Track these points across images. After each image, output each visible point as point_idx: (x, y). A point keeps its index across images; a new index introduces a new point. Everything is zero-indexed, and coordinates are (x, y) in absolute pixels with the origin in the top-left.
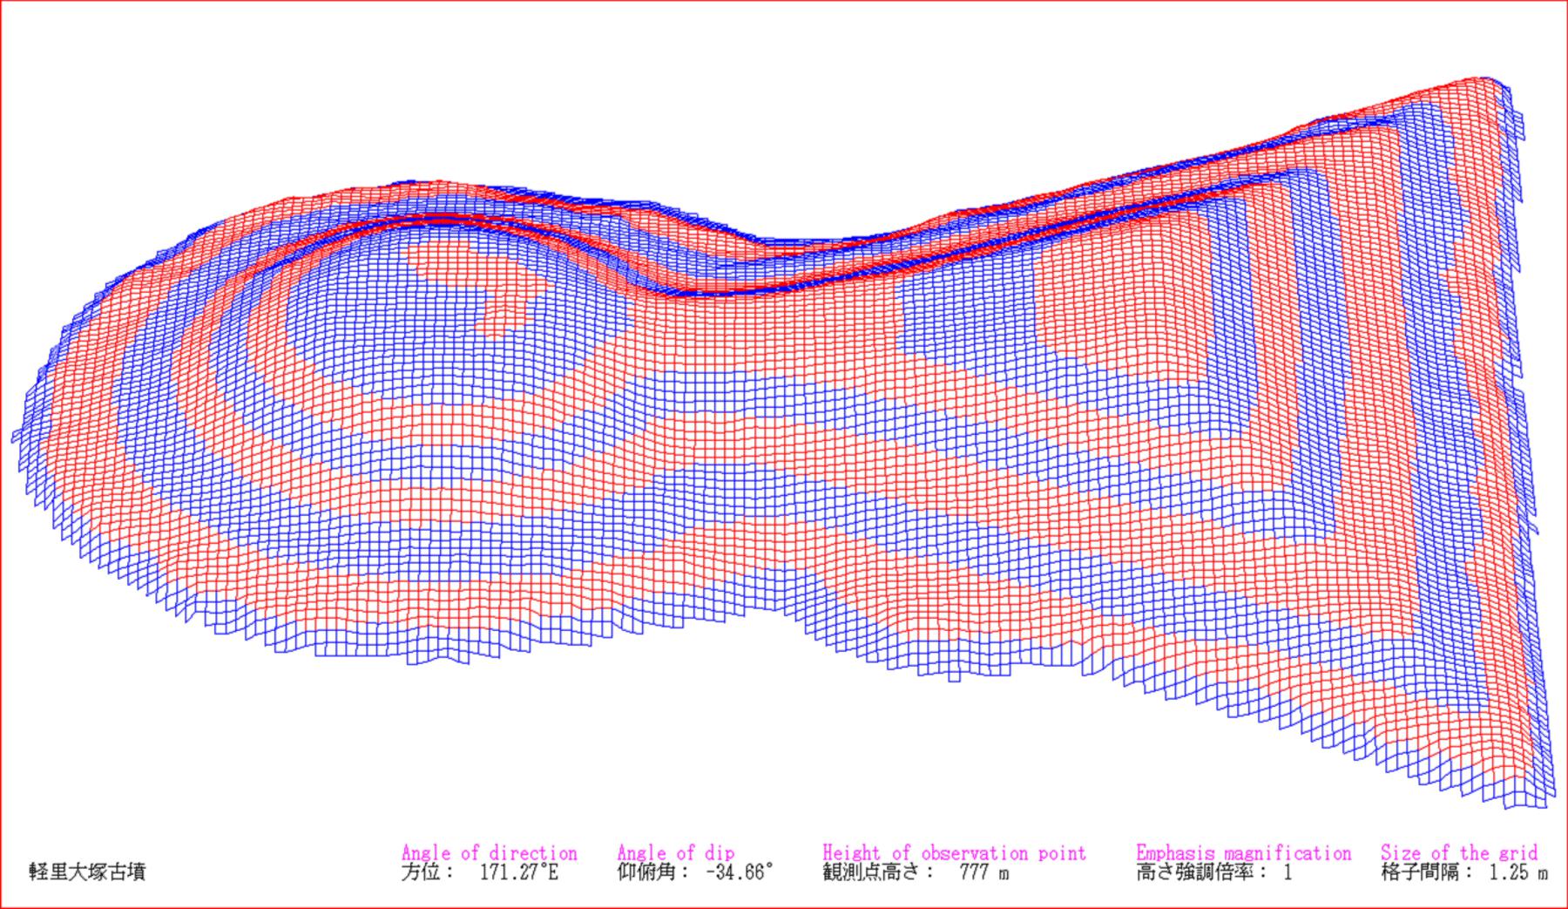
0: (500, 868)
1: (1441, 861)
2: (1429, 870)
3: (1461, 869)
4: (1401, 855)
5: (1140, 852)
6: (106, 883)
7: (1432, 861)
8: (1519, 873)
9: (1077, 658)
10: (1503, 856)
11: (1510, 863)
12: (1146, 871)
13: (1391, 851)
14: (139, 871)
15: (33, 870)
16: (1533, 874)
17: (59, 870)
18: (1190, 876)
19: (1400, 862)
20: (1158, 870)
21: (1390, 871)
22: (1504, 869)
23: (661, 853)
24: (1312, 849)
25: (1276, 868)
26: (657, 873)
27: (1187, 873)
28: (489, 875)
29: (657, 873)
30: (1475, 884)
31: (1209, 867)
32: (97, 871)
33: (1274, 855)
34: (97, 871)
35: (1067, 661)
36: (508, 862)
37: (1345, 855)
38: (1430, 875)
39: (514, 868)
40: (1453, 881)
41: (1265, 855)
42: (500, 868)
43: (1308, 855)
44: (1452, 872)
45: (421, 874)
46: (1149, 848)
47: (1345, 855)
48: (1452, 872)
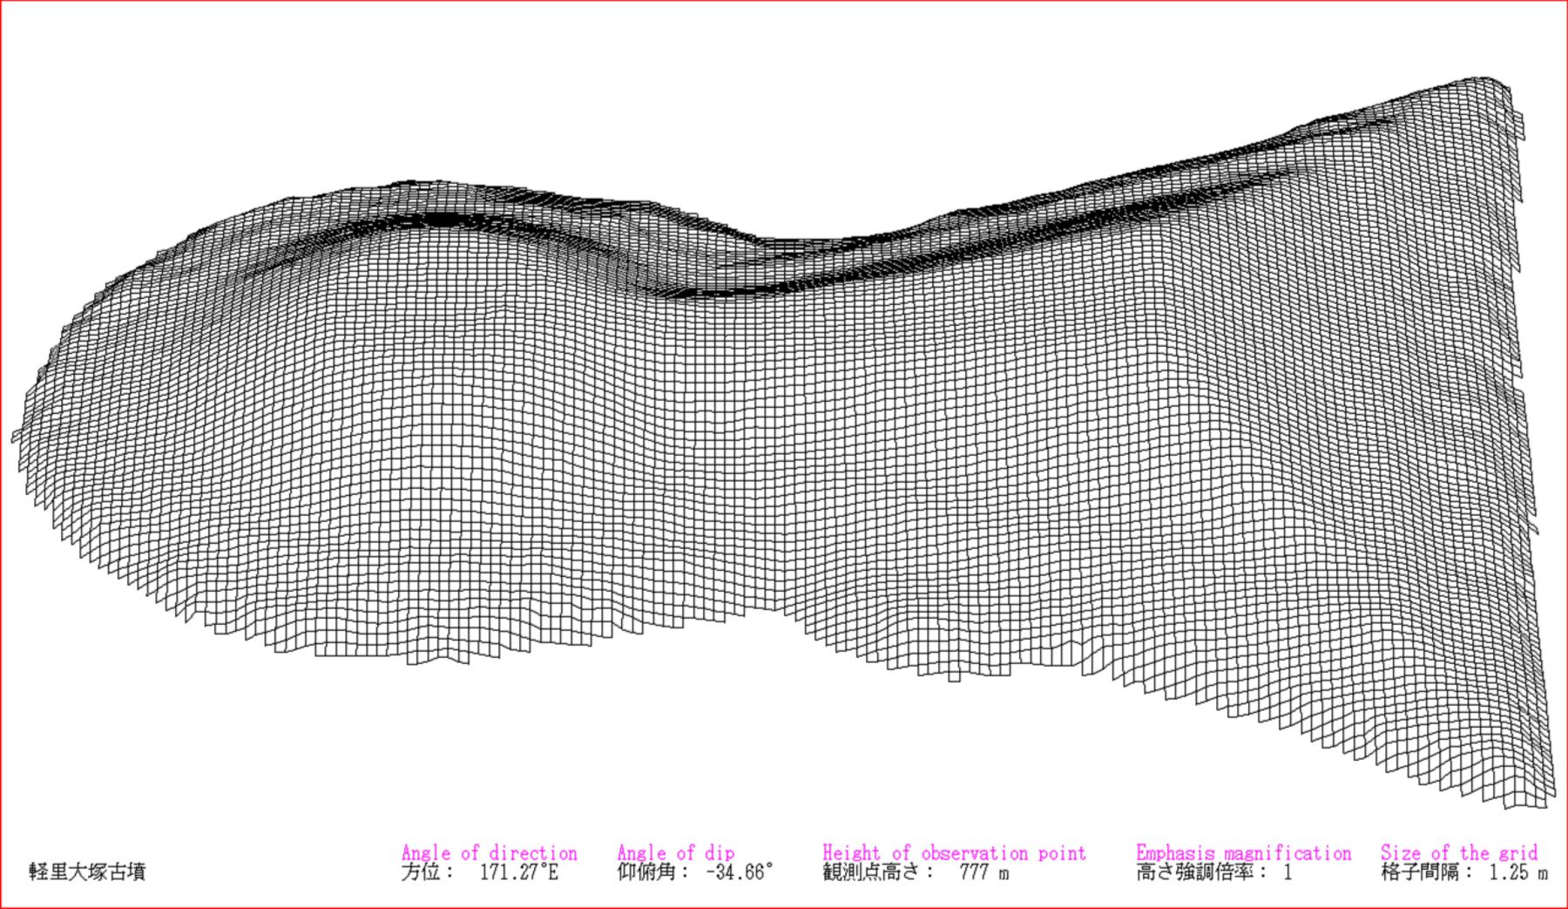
0: (500, 868)
1: (1441, 861)
2: (1429, 870)
3: (1461, 869)
4: (1401, 855)
5: (1140, 852)
6: (106, 883)
7: (1432, 861)
8: (1519, 873)
9: (1077, 658)
10: (1503, 856)
11: (1510, 863)
12: (1146, 871)
13: (1391, 851)
14: (139, 871)
15: (33, 870)
16: (1533, 874)
17: (59, 870)
18: (1190, 876)
19: (1400, 862)
20: (1158, 870)
21: (1390, 871)
22: (1504, 869)
23: (661, 853)
24: (1312, 849)
25: (1276, 868)
26: (657, 873)
27: (1187, 873)
28: (489, 875)
29: (657, 873)
30: (1475, 884)
31: (1209, 867)
32: (97, 871)
33: (1274, 855)
34: (97, 871)
35: (1067, 661)
36: (508, 862)
37: (1345, 855)
38: (1430, 875)
39: (514, 868)
40: (1453, 881)
41: (1265, 855)
42: (500, 868)
43: (1308, 855)
44: (1452, 872)
45: (421, 874)
46: (1149, 848)
47: (1345, 855)
48: (1452, 872)
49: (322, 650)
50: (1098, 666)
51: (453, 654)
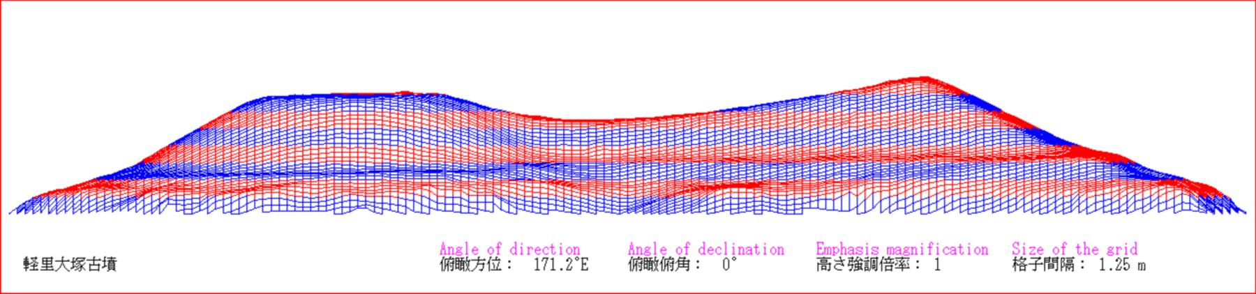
0: (550, 262)
1: (1060, 256)
2: (1051, 263)
3: (1076, 262)
4: (1028, 251)
5: (819, 248)
6: (85, 273)
7: (1053, 256)
8: (1123, 265)
9: (853, 205)
10: (1110, 252)
11: (1116, 257)
12: (824, 264)
13: (1020, 247)
14: (111, 264)
15: (26, 263)
16: (1134, 266)
17: (48, 263)
18: (859, 268)
19: (1028, 256)
20: (833, 263)
21: (1019, 264)
22: (1110, 262)
23: (475, 250)
24: (957, 246)
25: (928, 261)
26: (676, 266)
27: (857, 266)
28: (541, 267)
29: (676, 266)
30: (1087, 275)
31: (874, 260)
32: (78, 263)
33: (926, 251)
34: (78, 263)
35: (846, 207)
36: (557, 257)
37: (983, 251)
38: (1051, 266)
39: (561, 262)
40: (1070, 272)
41: (919, 251)
42: (550, 262)
43: (953, 251)
44: (1069, 264)
45: (486, 266)
46: (826, 245)
47: (983, 251)
48: (1069, 264)
49: (187, 210)
50: (869, 206)
51: (394, 208)
